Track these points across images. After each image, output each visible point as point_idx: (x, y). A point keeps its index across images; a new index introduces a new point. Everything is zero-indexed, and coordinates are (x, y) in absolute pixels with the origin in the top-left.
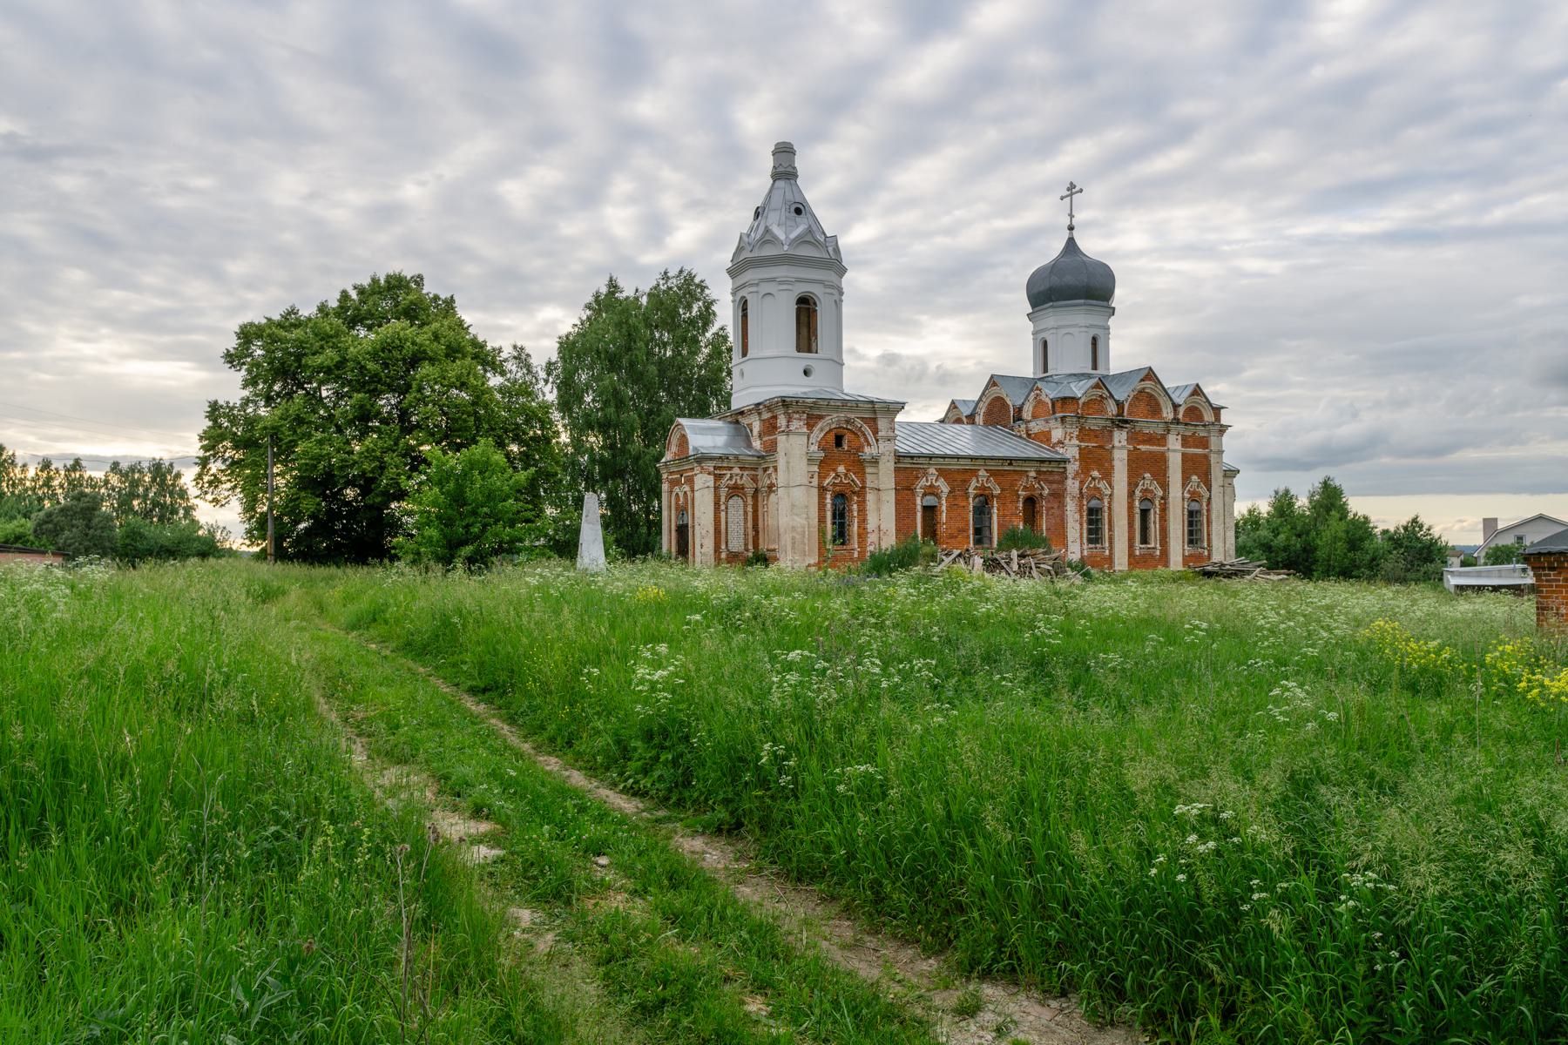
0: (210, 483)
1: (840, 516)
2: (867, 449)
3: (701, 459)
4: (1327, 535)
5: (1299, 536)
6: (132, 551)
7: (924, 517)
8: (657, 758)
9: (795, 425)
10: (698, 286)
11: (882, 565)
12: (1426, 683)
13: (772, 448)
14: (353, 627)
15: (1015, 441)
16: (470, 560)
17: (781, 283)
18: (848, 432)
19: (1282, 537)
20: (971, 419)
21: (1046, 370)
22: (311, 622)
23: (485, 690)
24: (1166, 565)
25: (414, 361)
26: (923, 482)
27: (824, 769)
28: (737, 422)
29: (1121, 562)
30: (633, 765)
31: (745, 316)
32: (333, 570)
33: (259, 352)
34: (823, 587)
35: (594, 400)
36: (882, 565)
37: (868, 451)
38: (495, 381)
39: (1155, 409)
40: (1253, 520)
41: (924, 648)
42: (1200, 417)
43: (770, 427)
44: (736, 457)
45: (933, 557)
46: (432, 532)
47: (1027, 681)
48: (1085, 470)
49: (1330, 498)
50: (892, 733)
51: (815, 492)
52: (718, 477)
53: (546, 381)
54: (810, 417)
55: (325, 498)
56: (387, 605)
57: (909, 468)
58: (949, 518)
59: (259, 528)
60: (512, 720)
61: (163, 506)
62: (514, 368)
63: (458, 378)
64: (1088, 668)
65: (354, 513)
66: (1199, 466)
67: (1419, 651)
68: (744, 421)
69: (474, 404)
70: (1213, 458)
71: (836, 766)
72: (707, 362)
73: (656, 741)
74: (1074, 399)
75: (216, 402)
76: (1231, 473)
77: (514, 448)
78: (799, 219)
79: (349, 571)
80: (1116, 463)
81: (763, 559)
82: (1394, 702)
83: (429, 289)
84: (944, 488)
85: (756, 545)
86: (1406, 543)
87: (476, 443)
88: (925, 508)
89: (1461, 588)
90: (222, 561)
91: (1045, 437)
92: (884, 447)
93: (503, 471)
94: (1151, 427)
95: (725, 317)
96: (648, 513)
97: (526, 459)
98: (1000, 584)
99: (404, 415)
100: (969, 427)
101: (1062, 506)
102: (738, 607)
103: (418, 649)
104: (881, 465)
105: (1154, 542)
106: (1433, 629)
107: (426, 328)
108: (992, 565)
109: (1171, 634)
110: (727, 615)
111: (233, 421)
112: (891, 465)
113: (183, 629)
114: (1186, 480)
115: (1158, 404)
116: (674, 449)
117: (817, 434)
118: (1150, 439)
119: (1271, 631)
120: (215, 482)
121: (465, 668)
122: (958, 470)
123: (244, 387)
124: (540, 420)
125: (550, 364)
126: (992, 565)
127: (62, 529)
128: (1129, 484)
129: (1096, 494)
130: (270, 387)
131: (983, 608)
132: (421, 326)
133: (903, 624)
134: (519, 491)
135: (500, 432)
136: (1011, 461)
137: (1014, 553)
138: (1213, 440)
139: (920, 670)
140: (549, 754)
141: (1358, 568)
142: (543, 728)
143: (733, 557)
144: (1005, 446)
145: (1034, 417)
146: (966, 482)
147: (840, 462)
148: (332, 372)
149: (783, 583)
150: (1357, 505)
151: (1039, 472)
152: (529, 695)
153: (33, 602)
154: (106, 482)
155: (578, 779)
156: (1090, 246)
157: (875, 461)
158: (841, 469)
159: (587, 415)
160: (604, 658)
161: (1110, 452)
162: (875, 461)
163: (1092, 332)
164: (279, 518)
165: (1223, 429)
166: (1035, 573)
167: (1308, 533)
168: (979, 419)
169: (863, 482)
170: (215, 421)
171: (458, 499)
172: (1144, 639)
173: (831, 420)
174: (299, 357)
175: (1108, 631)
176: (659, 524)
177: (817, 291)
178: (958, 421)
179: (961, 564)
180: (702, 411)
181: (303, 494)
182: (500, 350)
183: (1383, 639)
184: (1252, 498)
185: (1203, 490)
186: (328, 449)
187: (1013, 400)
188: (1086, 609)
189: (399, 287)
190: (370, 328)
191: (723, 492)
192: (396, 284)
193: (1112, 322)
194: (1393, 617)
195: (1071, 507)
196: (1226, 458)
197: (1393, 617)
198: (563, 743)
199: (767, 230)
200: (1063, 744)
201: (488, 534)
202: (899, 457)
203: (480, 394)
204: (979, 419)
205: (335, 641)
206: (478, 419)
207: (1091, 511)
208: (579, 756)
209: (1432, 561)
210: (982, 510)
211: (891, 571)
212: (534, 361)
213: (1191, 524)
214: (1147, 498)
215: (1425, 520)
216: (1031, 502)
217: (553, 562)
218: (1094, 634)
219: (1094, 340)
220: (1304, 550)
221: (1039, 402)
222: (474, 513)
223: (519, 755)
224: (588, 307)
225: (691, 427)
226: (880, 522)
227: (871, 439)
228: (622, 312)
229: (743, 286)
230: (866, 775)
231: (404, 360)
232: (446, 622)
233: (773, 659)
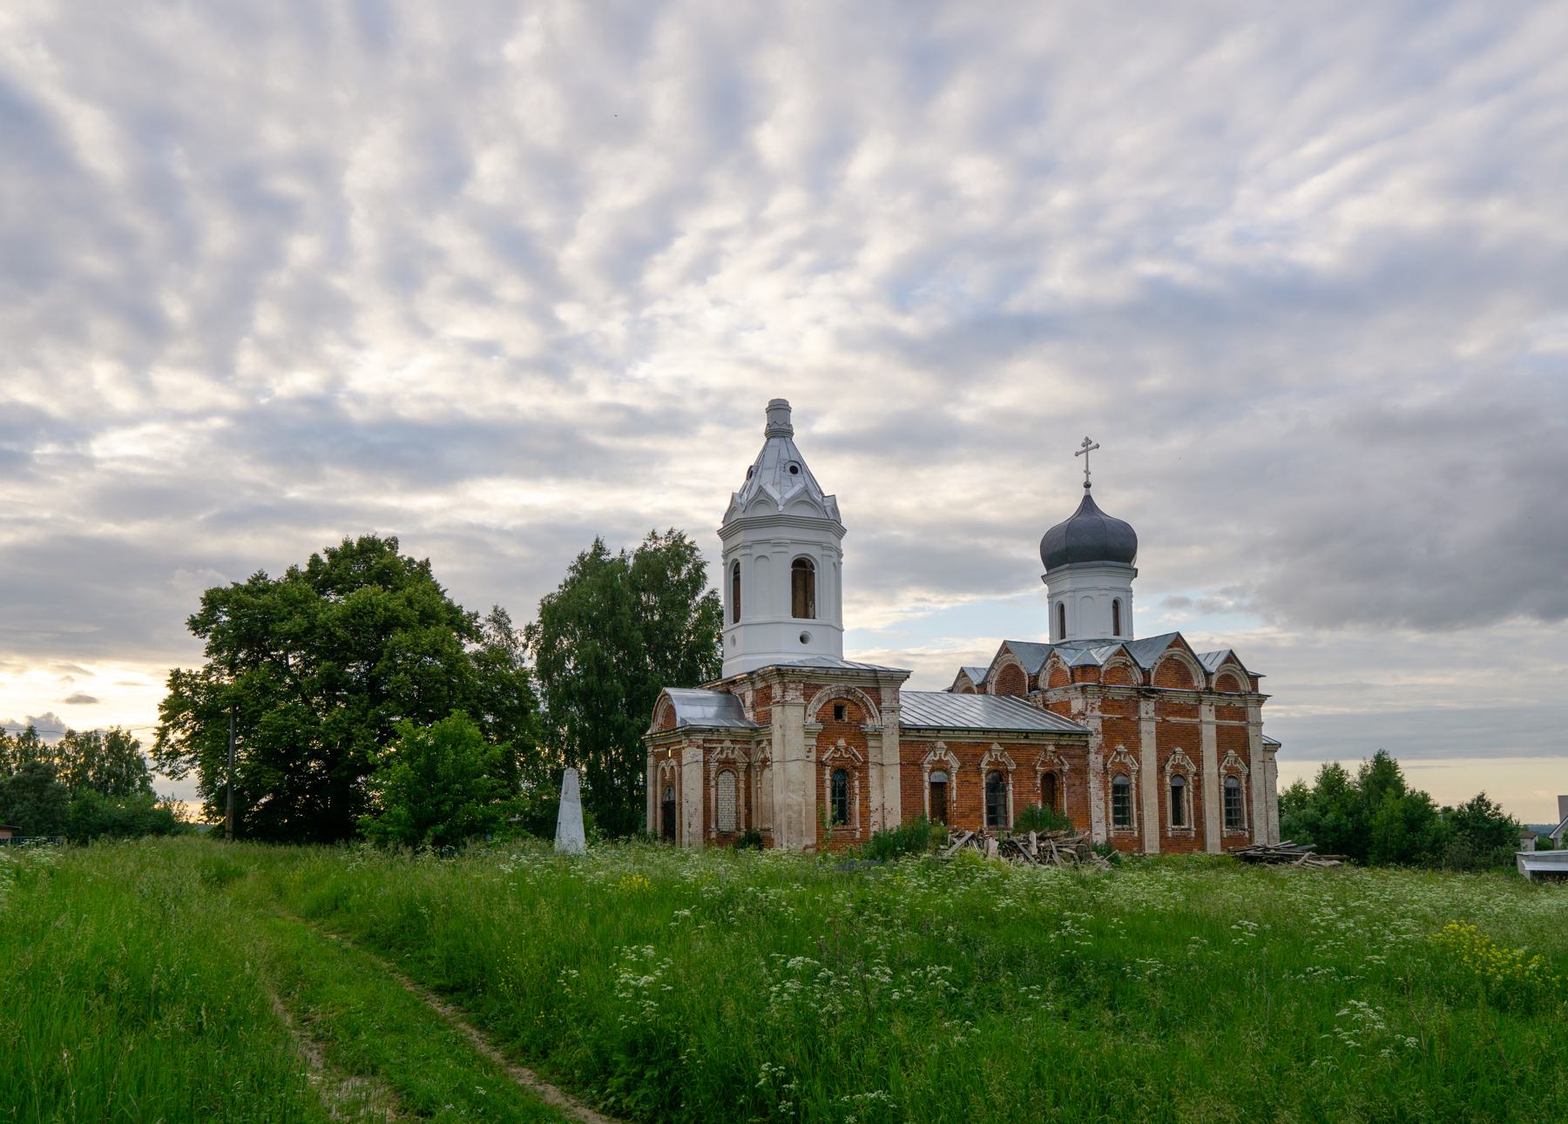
0: (168, 754)
1: (841, 795)
2: (869, 721)
3: (690, 731)
4: (1382, 815)
5: (1350, 815)
6: (84, 829)
8: (641, 1075)
9: (791, 695)
10: (687, 547)
11: (888, 848)
12: (1516, 999)
13: (766, 719)
14: (312, 915)
15: (1031, 712)
16: (439, 841)
19: (1331, 816)
20: (982, 688)
21: (1063, 636)
22: (269, 916)
23: (453, 990)
24: (1203, 848)
25: (387, 626)
26: (931, 757)
27: (830, 1094)
28: (729, 692)
29: (1152, 845)
30: (614, 1082)
31: (737, 580)
32: (294, 849)
33: (225, 618)
34: (823, 876)
35: (575, 668)
36: (888, 848)
38: (471, 647)
39: (1185, 678)
40: (1297, 796)
41: (940, 954)
42: (1235, 687)
43: (764, 698)
44: (727, 729)
45: (943, 840)
46: (400, 810)
47: (1056, 991)
48: (1109, 744)
49: (1384, 775)
50: (906, 1058)
51: (813, 767)
52: (707, 751)
54: (807, 686)
55: (288, 770)
56: (350, 891)
57: (915, 740)
58: (960, 795)
59: (218, 798)
60: (481, 1025)
61: (118, 777)
62: (492, 632)
63: (432, 645)
64: (1124, 974)
65: (318, 787)
66: (1239, 739)
67: (1508, 959)
68: (736, 691)
69: (447, 672)
70: (1251, 731)
71: (844, 1092)
72: (696, 628)
73: (641, 1054)
74: (1096, 667)
75: (178, 671)
76: (1272, 747)
77: (490, 718)
78: (794, 478)
79: (311, 850)
81: (757, 840)
82: (1481, 1018)
84: (955, 764)
86: (1472, 824)
87: (449, 714)
88: (933, 785)
89: (1540, 876)
90: (177, 839)
91: (1064, 708)
92: (887, 719)
93: (478, 744)
95: (716, 580)
96: (632, 787)
97: (501, 728)
98: (1021, 871)
99: (374, 683)
100: (980, 697)
102: (730, 901)
104: (885, 739)
105: (1189, 823)
106: (1516, 932)
107: (399, 593)
108: (1008, 849)
109: (1216, 932)
110: (718, 909)
111: (195, 689)
112: (896, 739)
113: (130, 925)
114: (1221, 756)
115: (1189, 673)
116: (660, 720)
117: (815, 706)
119: (1328, 929)
120: (174, 754)
121: (432, 963)
122: (968, 743)
123: (208, 655)
124: (517, 689)
126: (1008, 849)
127: (13, 802)
128: (1159, 759)
129: (1124, 771)
130: (235, 654)
131: (1004, 903)
132: (394, 591)
133: (915, 921)
134: (493, 765)
135: (474, 702)
136: (1027, 734)
137: (1033, 836)
138: (1251, 710)
139: (934, 979)
140: (522, 1065)
141: (1419, 851)
142: (515, 1034)
143: (724, 838)
144: (1020, 718)
145: (1051, 686)
146: (979, 757)
147: (840, 735)
148: (298, 640)
149: (779, 871)
150: (1417, 776)
151: (1058, 746)
152: (498, 996)
154: (61, 751)
155: (553, 1095)
156: (1112, 505)
158: (841, 742)
159: (567, 684)
160: (584, 958)
162: (878, 735)
163: (1113, 595)
164: (240, 791)
165: (1261, 699)
166: (1056, 857)
167: (1360, 811)
168: (991, 688)
169: (866, 756)
170: (176, 690)
171: (428, 773)
172: (1186, 941)
174: (265, 624)
175: (1147, 929)
176: (643, 800)
177: (814, 553)
178: (969, 690)
179: (975, 848)
180: (689, 679)
181: (265, 767)
182: (477, 616)
183: (1460, 944)
184: (1296, 773)
185: (1241, 766)
186: (292, 719)
187: (1029, 667)
188: (1117, 901)
189: (372, 551)
190: (340, 592)
191: (713, 767)
192: (370, 547)
193: (1134, 584)
194: (1467, 916)
195: (1094, 784)
196: (1265, 731)
197: (1467, 916)
198: (539, 1052)
199: (761, 490)
200: (1103, 1074)
201: (460, 813)
202: (904, 730)
203: (455, 663)
204: (991, 688)
206: (452, 687)
207: (1117, 789)
208: (555, 1069)
209: (1503, 843)
210: (996, 786)
211: (896, 856)
213: (1228, 802)
215: (1493, 798)
216: (1050, 779)
217: (528, 843)
218: (1129, 933)
219: (1116, 604)
220: (1357, 830)
221: (1056, 670)
223: (489, 1066)
225: (679, 698)
226: (885, 800)
227: (874, 711)
228: (607, 575)
229: (735, 548)
230: (876, 1103)
231: (375, 626)
232: (414, 914)
233: (771, 963)
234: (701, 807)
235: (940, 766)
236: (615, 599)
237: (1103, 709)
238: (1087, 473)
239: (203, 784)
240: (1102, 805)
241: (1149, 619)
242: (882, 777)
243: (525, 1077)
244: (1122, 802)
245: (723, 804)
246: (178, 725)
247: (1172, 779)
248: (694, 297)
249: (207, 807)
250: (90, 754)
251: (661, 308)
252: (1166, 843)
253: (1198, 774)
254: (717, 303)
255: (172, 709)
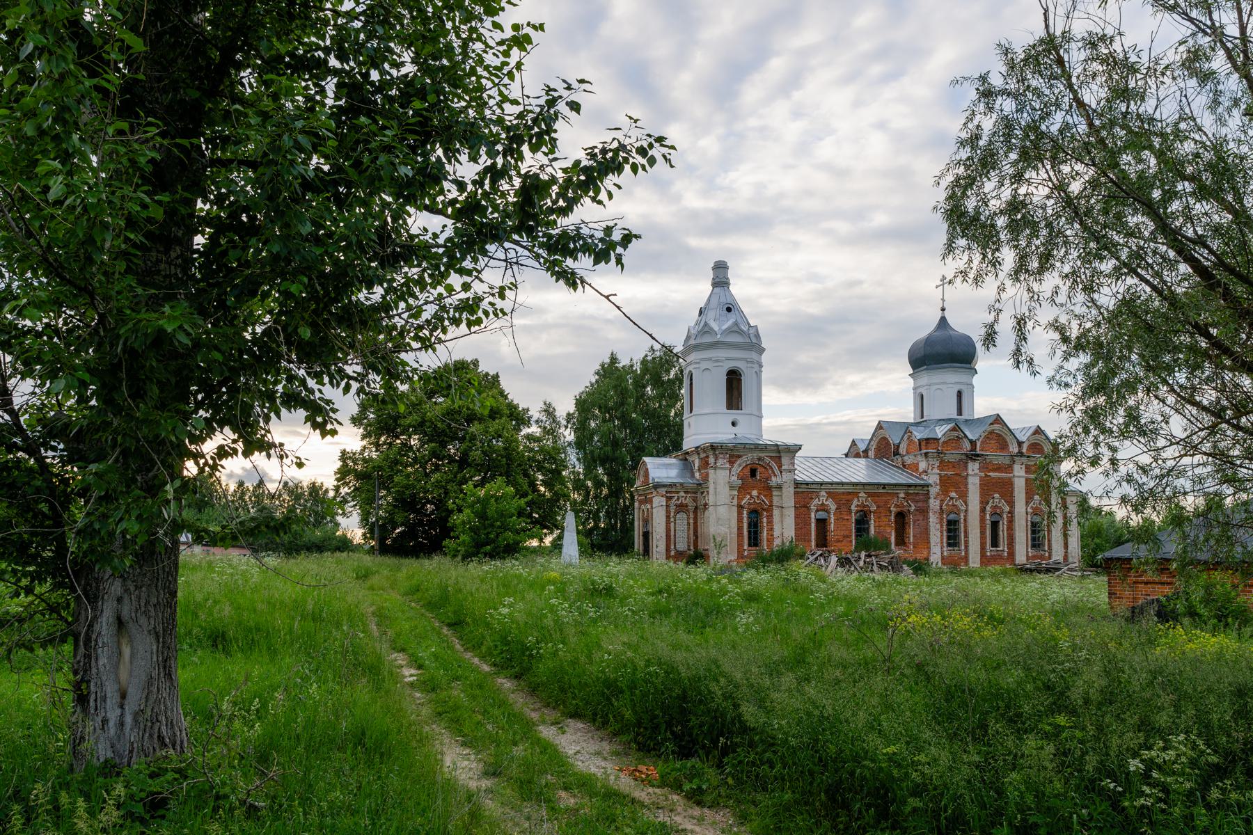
3: (657, 486)
7: (817, 526)
14: (406, 594)
17: (717, 361)
18: (761, 465)
20: (866, 453)
26: (816, 502)
29: (975, 561)
37: (774, 480)
39: (1003, 445)
43: (705, 464)
44: (682, 484)
51: (735, 509)
52: (669, 499)
53: (566, 427)
54: (731, 456)
57: (805, 491)
58: (837, 528)
59: (371, 529)
60: (461, 638)
61: (316, 513)
68: (690, 459)
74: (937, 440)
78: (729, 315)
80: (970, 486)
83: (483, 368)
84: (833, 507)
85: (696, 546)
88: (818, 521)
91: (915, 467)
92: (786, 477)
94: (999, 458)
101: (926, 518)
103: (432, 606)
105: (1003, 546)
111: (355, 461)
112: (792, 490)
114: (1029, 498)
116: (641, 478)
117: (737, 469)
118: (999, 469)
122: (843, 493)
125: (569, 414)
128: (981, 502)
136: (884, 486)
137: (863, 554)
146: (849, 502)
151: (907, 494)
153: (244, 574)
157: (779, 487)
158: (755, 493)
161: (966, 478)
162: (779, 487)
163: (957, 388)
164: (384, 525)
166: (875, 568)
168: (871, 454)
169: (771, 501)
173: (747, 458)
178: (857, 455)
185: (1045, 508)
187: (894, 439)
191: (673, 509)
195: (933, 519)
199: (706, 324)
202: (797, 484)
204: (871, 454)
205: (392, 599)
207: (950, 523)
212: (558, 414)
213: (1033, 532)
214: (996, 513)
216: (901, 517)
219: (960, 394)
222: (492, 525)
224: (597, 373)
227: (777, 471)
234: (735, 536)
235: (822, 508)
236: (623, 393)
237: (941, 468)
238: (943, 300)
239: (362, 521)
240: (939, 534)
241: (982, 405)
242: (782, 516)
243: (506, 684)
244: (953, 533)
245: (679, 533)
246: (347, 484)
247: (991, 515)
248: (779, 113)
249: (364, 535)
250: (298, 497)
251: (753, 122)
252: (985, 560)
253: (1011, 513)
254: (797, 114)
255: (343, 473)
